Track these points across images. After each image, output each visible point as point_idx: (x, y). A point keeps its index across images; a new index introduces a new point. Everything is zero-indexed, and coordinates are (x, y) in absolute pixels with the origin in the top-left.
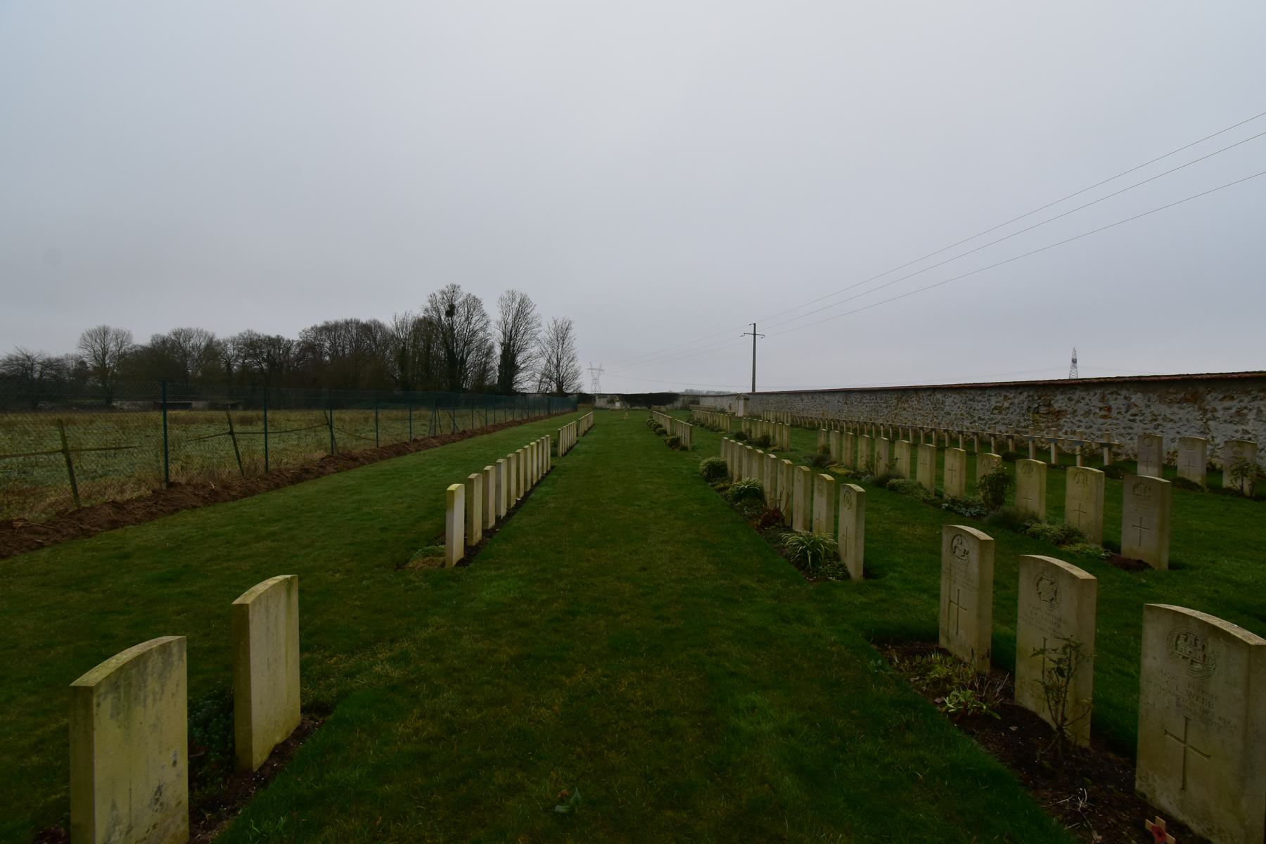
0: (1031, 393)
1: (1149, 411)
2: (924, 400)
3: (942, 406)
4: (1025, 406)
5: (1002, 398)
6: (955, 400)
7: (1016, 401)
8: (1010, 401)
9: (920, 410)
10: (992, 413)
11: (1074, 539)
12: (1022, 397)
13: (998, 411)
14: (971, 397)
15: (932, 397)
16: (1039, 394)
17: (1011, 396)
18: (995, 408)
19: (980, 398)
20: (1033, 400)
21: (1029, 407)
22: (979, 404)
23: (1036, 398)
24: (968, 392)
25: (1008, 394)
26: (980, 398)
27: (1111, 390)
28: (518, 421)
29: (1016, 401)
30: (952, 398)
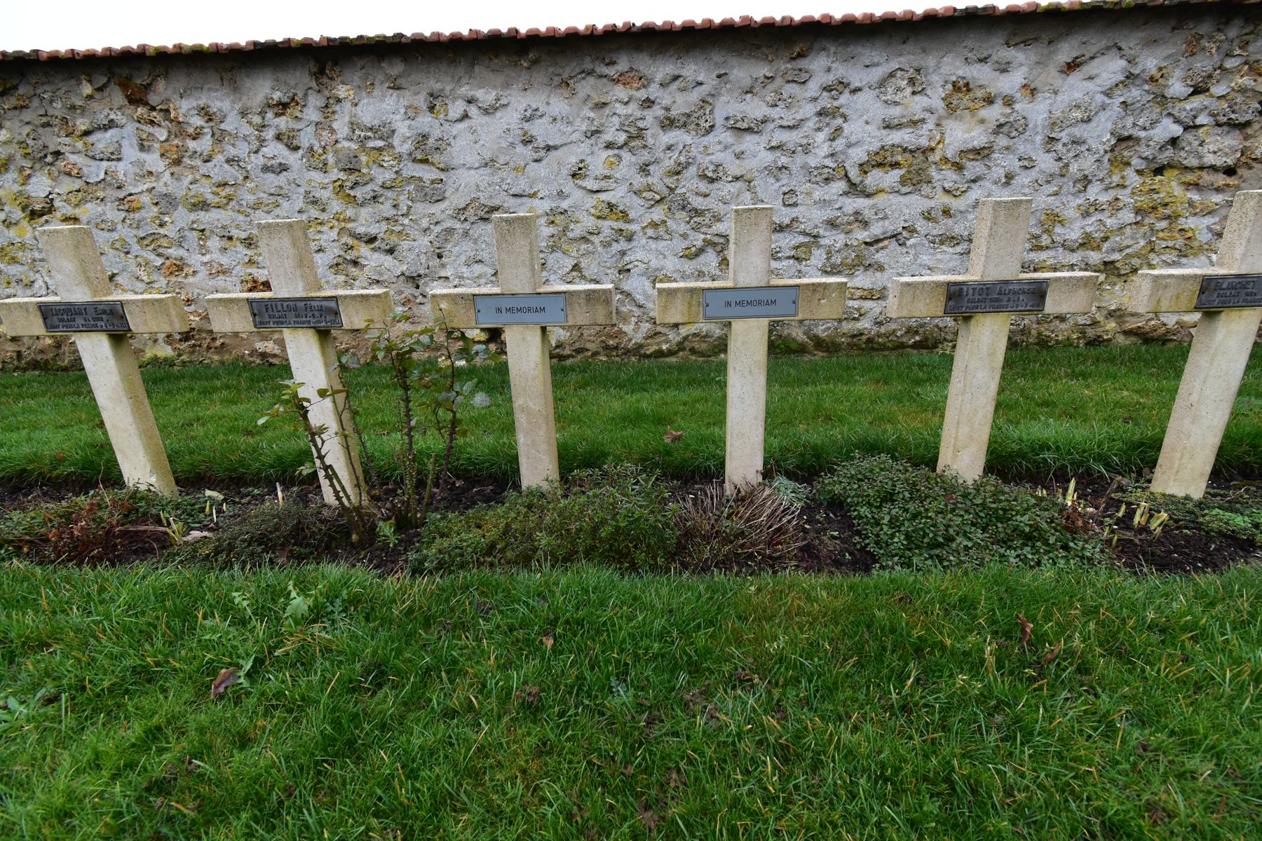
0: (1150, 63)
1: (650, 179)
2: (219, 138)
3: (428, 174)
4: (1099, 134)
5: (935, 98)
6: (539, 129)
7: (1037, 112)
8: (995, 113)
9: (202, 205)
10: (854, 189)
11: (718, 715)
12: (1076, 88)
13: (896, 174)
14: (682, 102)
15: (312, 114)
16: (1203, 64)
17: (1010, 83)
18: (880, 161)
19: (755, 108)
20: (1161, 99)
21: (1124, 140)
22: (749, 142)
23: (1177, 87)
24: (661, 69)
25: (980, 74)
26: (755, 108)
27: (1170, 52)
28: (166, 359)
29: (1037, 112)
30: (510, 118)
